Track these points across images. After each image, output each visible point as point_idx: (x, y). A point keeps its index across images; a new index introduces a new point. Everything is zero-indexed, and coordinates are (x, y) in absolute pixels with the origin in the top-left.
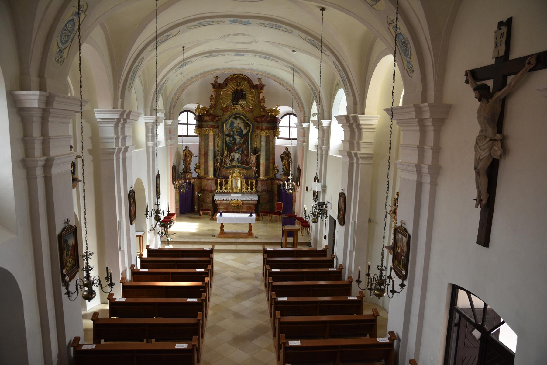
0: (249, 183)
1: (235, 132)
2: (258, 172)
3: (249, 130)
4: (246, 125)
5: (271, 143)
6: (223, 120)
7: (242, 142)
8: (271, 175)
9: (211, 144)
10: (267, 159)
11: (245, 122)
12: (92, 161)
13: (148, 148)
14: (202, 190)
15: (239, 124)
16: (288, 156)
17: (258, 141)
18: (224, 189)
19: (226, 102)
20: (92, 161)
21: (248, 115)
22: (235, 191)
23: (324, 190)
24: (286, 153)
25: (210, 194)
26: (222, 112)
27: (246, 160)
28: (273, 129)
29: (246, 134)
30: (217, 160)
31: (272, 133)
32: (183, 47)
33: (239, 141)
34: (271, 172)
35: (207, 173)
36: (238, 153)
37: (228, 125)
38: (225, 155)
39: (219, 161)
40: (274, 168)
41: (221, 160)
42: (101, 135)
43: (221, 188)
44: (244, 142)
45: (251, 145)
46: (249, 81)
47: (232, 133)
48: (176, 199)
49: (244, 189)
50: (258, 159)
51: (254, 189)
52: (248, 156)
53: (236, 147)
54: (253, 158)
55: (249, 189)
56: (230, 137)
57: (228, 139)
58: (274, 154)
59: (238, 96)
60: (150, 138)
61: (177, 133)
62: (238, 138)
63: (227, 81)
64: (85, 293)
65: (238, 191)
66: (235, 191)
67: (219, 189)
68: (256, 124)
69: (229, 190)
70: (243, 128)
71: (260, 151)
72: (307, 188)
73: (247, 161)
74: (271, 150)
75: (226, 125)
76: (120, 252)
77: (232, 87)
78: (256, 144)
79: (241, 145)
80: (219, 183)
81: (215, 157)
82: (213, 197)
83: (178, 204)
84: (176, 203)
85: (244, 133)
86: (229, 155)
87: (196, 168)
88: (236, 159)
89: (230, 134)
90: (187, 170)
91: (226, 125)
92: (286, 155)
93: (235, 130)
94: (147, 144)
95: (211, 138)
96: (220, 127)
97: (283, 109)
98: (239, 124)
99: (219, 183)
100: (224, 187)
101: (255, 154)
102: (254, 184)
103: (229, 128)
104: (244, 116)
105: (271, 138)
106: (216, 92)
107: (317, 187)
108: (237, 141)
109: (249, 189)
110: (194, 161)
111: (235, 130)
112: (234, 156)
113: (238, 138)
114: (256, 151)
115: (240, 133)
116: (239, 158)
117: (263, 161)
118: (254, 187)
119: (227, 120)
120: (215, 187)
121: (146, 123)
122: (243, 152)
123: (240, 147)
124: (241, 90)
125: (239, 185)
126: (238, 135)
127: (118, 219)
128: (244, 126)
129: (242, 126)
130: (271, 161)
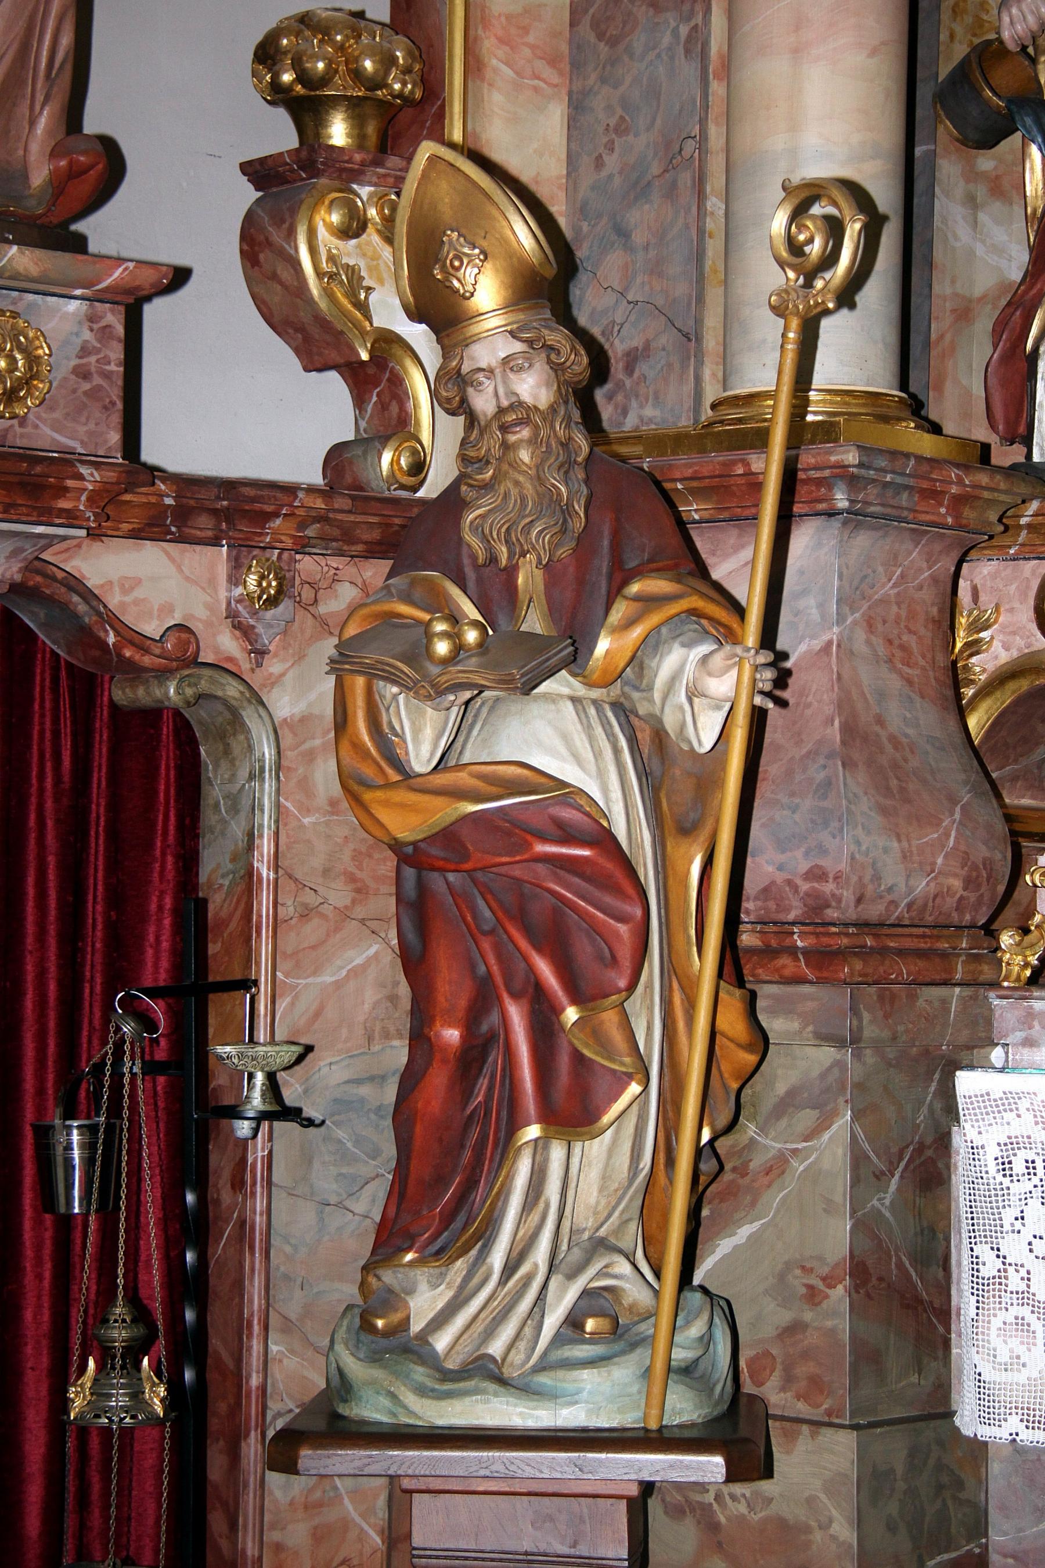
87: (280, 184)
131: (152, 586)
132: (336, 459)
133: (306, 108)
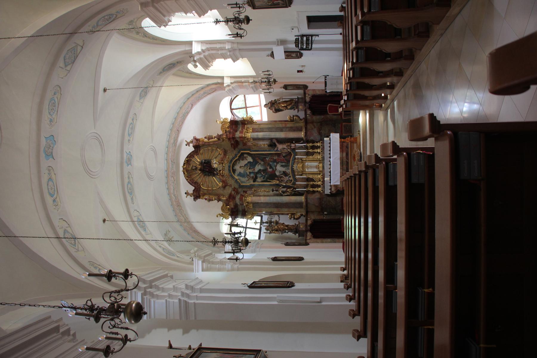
0: (311, 151)
1: (251, 171)
2: (298, 140)
3: (248, 154)
5: (262, 126)
6: (237, 186)
7: (262, 163)
8: (302, 124)
9: (263, 199)
10: (281, 130)
11: (239, 159)
12: (197, 330)
13: (233, 270)
14: (322, 209)
15: (241, 167)
16: (274, 104)
17: (261, 143)
18: (319, 183)
19: (216, 182)
20: (197, 330)
21: (230, 156)
22: (321, 169)
23: (282, 42)
24: (271, 106)
26: (227, 187)
27: (284, 157)
28: (245, 124)
29: (253, 158)
30: (283, 192)
31: (249, 126)
32: (104, 221)
33: (262, 165)
34: (297, 125)
35: (298, 205)
36: (276, 166)
37: (243, 179)
38: (278, 182)
39: (285, 189)
41: (284, 187)
42: (164, 317)
43: (318, 186)
44: (262, 160)
45: (266, 151)
46: (190, 156)
48: (331, 242)
50: (281, 141)
51: (318, 144)
52: (279, 155)
54: (280, 147)
55: (319, 151)
56: (256, 178)
58: (275, 121)
59: (207, 169)
60: (222, 266)
61: (256, 240)
62: (258, 168)
63: (191, 182)
64: (133, 322)
65: (321, 165)
66: (321, 169)
67: (319, 189)
68: (240, 147)
70: (246, 162)
71: (271, 139)
72: (298, 71)
73: (286, 156)
74: (270, 126)
75: (244, 182)
76: (323, 303)
77: (198, 177)
78: (264, 144)
79: (266, 163)
80: (311, 189)
82: (327, 195)
83: (337, 240)
84: (335, 242)
85: (252, 161)
86: (279, 178)
87: (294, 219)
88: (283, 169)
89: (253, 177)
91: (242, 182)
92: (273, 106)
93: (248, 171)
94: (228, 271)
95: (255, 199)
96: (245, 190)
97: (225, 114)
98: (241, 167)
99: (311, 189)
100: (316, 183)
101: (275, 146)
102: (311, 144)
103: (247, 179)
104: (231, 161)
105: (255, 127)
106: (204, 194)
107: (279, 52)
108: (262, 168)
109: (319, 151)
110: (286, 220)
111: (248, 171)
112: (280, 172)
113: (258, 168)
114: (273, 143)
116: (282, 166)
117: (281, 135)
118: (316, 144)
121: (203, 270)
122: (275, 161)
123: (269, 165)
124: (201, 163)
125: (316, 164)
126: (254, 168)
127: (276, 303)
128: (243, 160)
129: (243, 163)
130: (284, 125)
131: (309, 222)
132: (304, 216)
133: (292, 217)
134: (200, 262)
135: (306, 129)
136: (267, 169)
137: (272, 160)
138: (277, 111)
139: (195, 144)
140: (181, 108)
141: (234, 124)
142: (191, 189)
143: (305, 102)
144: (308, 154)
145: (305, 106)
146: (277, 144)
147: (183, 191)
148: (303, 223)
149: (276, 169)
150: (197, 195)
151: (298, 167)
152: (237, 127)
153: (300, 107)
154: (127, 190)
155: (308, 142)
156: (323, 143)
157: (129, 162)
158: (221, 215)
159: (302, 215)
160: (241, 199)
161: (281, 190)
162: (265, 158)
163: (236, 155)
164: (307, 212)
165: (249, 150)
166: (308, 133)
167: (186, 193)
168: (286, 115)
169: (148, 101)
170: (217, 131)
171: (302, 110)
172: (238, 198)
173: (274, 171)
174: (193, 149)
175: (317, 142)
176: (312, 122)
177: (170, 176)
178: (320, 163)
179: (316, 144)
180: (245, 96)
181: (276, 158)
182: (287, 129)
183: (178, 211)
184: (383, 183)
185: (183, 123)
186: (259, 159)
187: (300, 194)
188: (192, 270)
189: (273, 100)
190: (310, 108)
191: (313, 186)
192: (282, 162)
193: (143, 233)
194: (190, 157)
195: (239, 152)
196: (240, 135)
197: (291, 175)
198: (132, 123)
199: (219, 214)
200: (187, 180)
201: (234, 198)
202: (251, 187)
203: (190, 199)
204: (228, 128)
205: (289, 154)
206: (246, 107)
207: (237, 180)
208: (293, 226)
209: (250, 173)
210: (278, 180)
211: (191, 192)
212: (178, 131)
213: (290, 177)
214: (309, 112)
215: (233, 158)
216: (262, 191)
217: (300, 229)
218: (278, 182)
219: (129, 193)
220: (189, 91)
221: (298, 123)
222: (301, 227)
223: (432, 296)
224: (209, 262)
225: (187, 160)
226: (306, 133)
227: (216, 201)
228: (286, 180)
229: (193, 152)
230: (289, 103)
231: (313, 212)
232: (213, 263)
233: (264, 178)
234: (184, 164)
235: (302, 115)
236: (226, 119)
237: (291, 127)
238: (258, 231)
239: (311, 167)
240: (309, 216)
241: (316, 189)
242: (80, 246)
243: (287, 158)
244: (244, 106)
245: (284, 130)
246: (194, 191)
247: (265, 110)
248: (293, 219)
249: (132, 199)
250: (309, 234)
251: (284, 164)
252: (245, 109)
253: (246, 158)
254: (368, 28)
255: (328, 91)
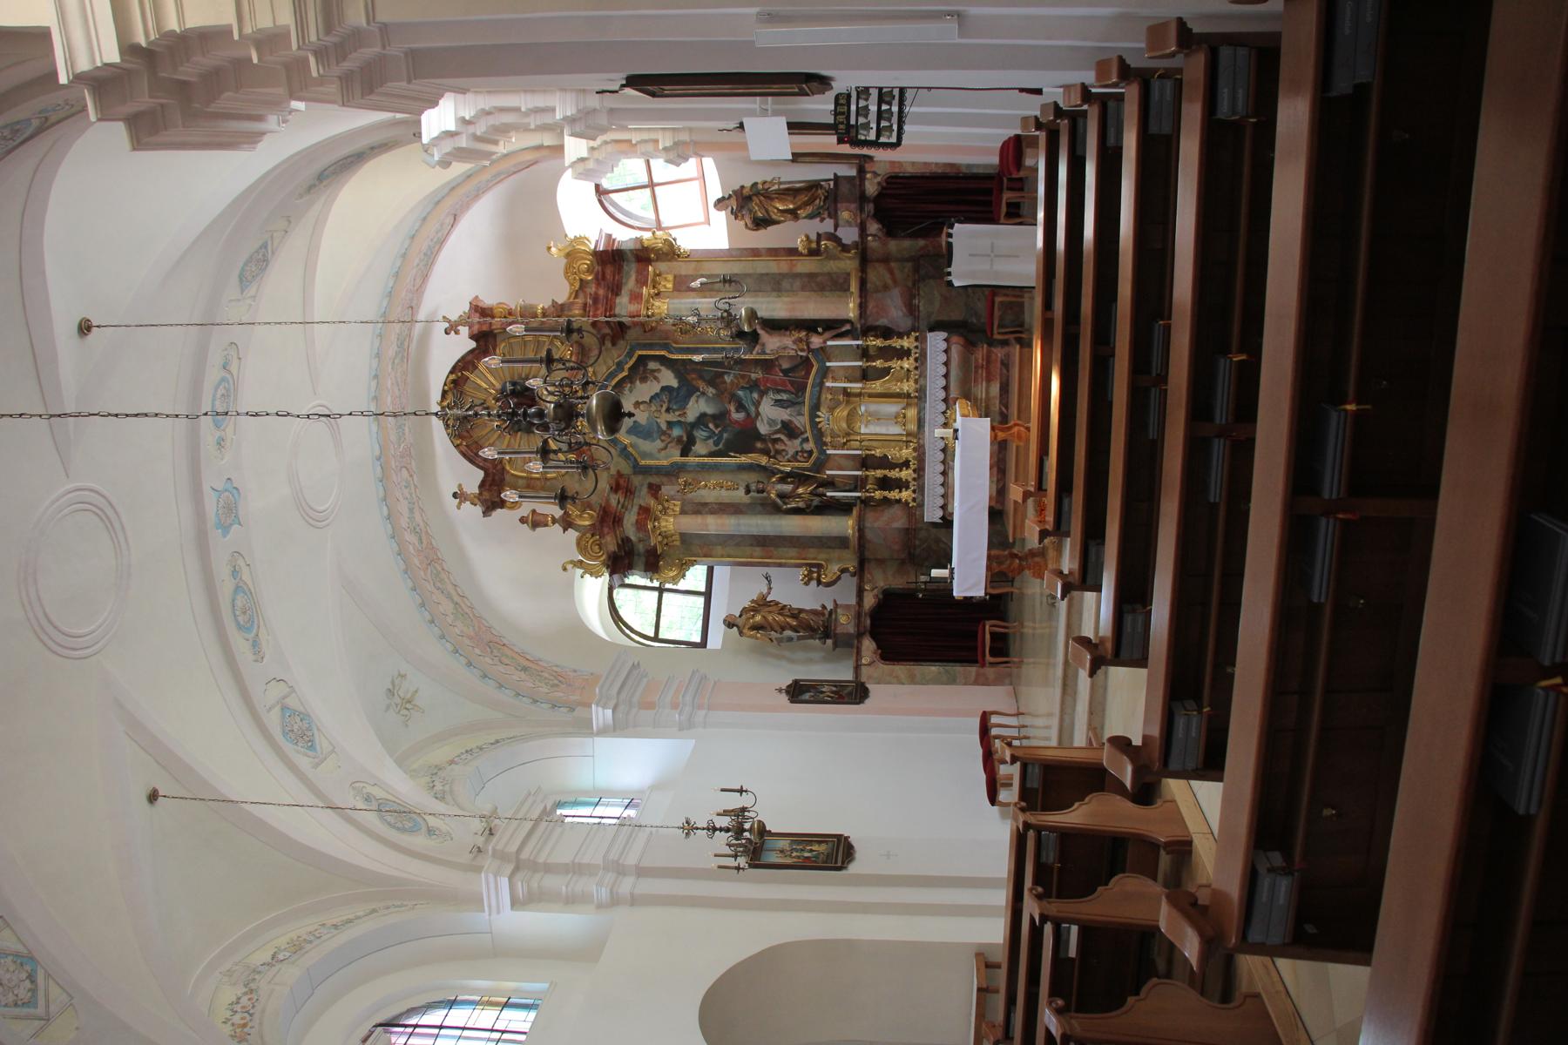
0: (878, 363)
1: (672, 417)
2: (832, 326)
3: (662, 360)
4: (639, 371)
6: (625, 468)
7: (711, 391)
11: (630, 379)
13: (615, 901)
16: (749, 198)
18: (905, 474)
24: (741, 207)
25: (923, 534)
27: (785, 372)
28: (648, 261)
29: (679, 375)
30: (782, 496)
31: (662, 266)
32: (153, 797)
33: (708, 400)
34: (833, 266)
35: (841, 542)
36: (757, 404)
37: (646, 445)
38: (764, 460)
39: (788, 488)
40: (813, 253)
41: (784, 478)
43: (901, 485)
44: (711, 383)
46: (465, 365)
47: (676, 432)
49: (907, 387)
50: (775, 326)
51: (906, 343)
52: (767, 365)
53: (738, 416)
54: (772, 343)
57: (700, 448)
62: (697, 407)
63: (471, 454)
65: (912, 413)
66: (913, 427)
67: (905, 495)
69: (906, 453)
70: (655, 388)
79: (723, 394)
80: (878, 494)
81: (774, 509)
82: (934, 524)
84: (952, 681)
85: (674, 383)
86: (769, 446)
88: (783, 414)
89: (679, 440)
90: (816, 628)
91: (645, 455)
92: (748, 204)
94: (600, 906)
96: (655, 480)
99: (878, 494)
103: (658, 444)
108: (710, 410)
110: (793, 591)
112: (772, 422)
113: (697, 407)
115: (675, 398)
116: (778, 403)
117: (774, 307)
118: (896, 343)
119: (624, 453)
120: (896, 511)
122: (754, 386)
123: (734, 397)
125: (891, 408)
126: (683, 407)
128: (644, 380)
131: (869, 601)
132: (853, 575)
133: (811, 579)
134: (504, 882)
135: (863, 283)
136: (728, 412)
137: (743, 383)
138: (760, 223)
139: (476, 329)
140: (413, 237)
141: (611, 260)
142: (473, 478)
143: (862, 198)
144: (865, 375)
145: (862, 210)
146: (760, 331)
147: (448, 486)
148: (847, 607)
149: (758, 414)
150: (491, 496)
151: (832, 420)
152: (620, 270)
153: (845, 215)
154: (235, 616)
155: (867, 331)
156: (921, 340)
157: (231, 513)
158: (580, 564)
159: (843, 571)
160: (640, 526)
161: (775, 489)
162: (721, 375)
163: (620, 366)
164: (862, 563)
165: (666, 347)
166: (871, 305)
167: (455, 495)
168: (794, 233)
169: (280, 282)
170: (551, 289)
171: (849, 224)
172: (630, 519)
173: (751, 421)
174: (473, 344)
175: (900, 336)
176: (886, 260)
177: (399, 470)
178: (908, 405)
179: (896, 343)
180: (648, 163)
181: (756, 375)
182: (798, 283)
183: (430, 587)
184: (1122, 451)
185: (425, 277)
186: (701, 377)
187: (843, 508)
188: (475, 901)
189: (748, 184)
190: (879, 216)
191: (885, 484)
192: (778, 391)
193: (304, 762)
194: (465, 368)
195: (630, 355)
196: (633, 308)
197: (808, 434)
198: (223, 380)
199: (571, 562)
200: (457, 447)
201: (617, 521)
202: (673, 472)
203: (473, 511)
204: (589, 271)
205: (806, 363)
206: (652, 185)
207: (625, 448)
208: (814, 612)
209: (670, 424)
210: (766, 452)
211: (472, 487)
212: (419, 290)
213: (807, 440)
214: (873, 227)
215: (611, 376)
216: (710, 491)
217: (839, 630)
218: (764, 460)
219: (240, 627)
220: (443, 181)
221: (835, 258)
222: (843, 620)
223: (1168, 328)
224: (534, 867)
225: (454, 382)
226: (862, 307)
227: (558, 528)
228: (791, 452)
229: (472, 351)
230: (804, 198)
231: (881, 562)
232: (548, 868)
233: (716, 444)
234: (444, 393)
235: (849, 235)
236: (580, 240)
237: (811, 276)
238: (701, 600)
239: (878, 418)
240: (867, 576)
241: (894, 495)
242: (55, 991)
243: (795, 379)
244: (644, 180)
245: (785, 284)
246: (482, 486)
247: (720, 218)
248: (814, 583)
249: (255, 644)
250: (868, 645)
251: (785, 397)
252: (648, 191)
253: (653, 374)
254: (1284, 885)
255: (957, 283)
